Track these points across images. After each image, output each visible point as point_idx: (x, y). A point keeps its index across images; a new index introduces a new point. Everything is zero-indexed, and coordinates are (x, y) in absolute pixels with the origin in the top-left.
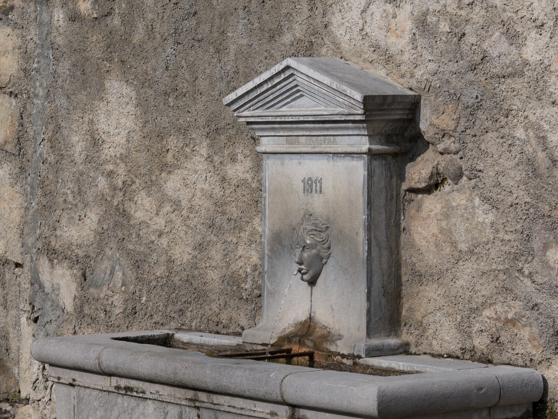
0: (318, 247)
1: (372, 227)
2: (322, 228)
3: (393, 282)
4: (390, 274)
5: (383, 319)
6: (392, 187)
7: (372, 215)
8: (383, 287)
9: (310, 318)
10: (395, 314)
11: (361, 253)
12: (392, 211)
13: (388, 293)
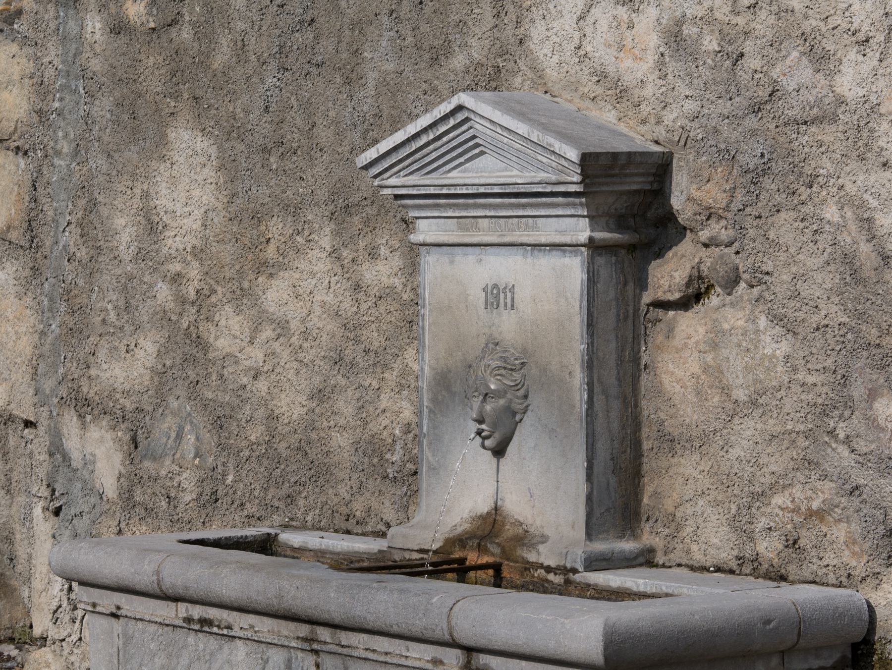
0: (509, 396)
1: (595, 364)
2: (515, 365)
3: (628, 450)
4: (623, 438)
5: (612, 511)
6: (626, 298)
7: (595, 345)
8: (612, 459)
9: (496, 509)
10: (632, 502)
11: (577, 405)
12: (626, 338)
13: (621, 468)
